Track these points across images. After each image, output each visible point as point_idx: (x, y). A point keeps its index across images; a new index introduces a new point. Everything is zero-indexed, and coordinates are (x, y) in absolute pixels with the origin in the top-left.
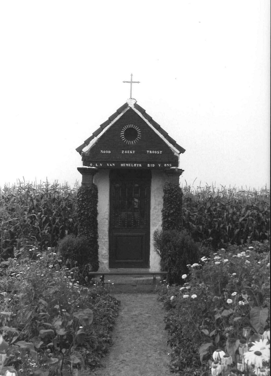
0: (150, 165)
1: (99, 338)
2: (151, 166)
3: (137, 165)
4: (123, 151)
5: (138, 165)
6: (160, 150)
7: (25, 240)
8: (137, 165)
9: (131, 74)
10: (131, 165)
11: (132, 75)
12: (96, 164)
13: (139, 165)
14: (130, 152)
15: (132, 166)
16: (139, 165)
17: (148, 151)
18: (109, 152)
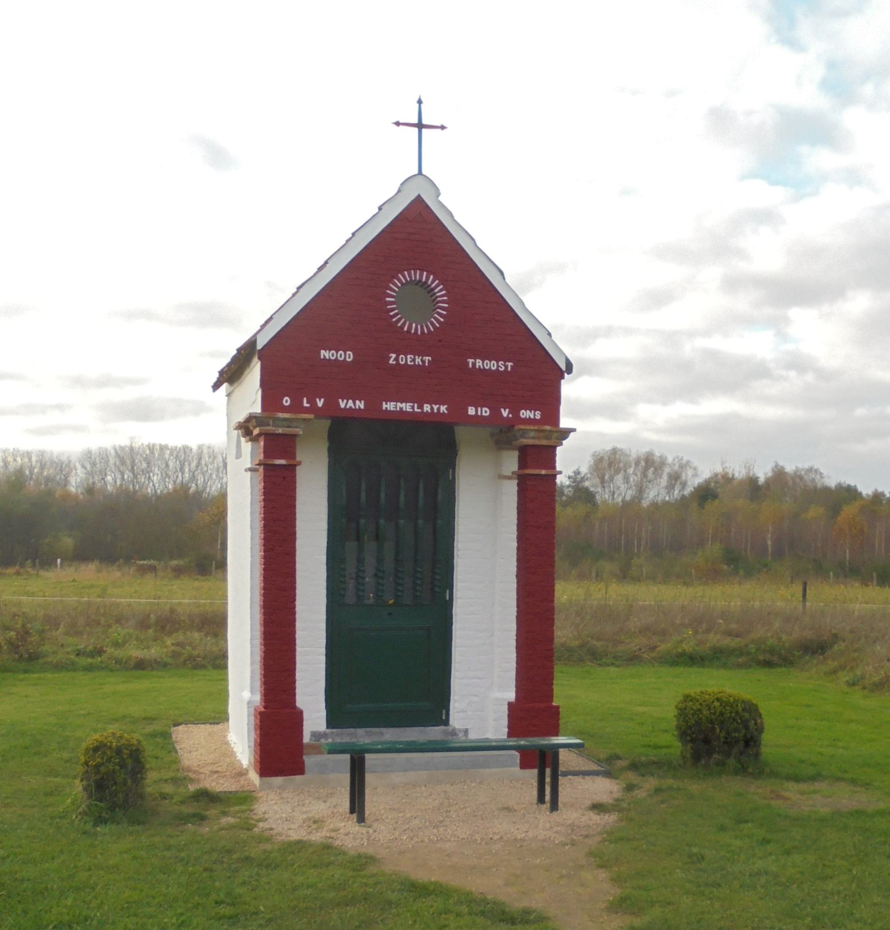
0: (476, 411)
1: (809, 98)
2: (479, 413)
3: (432, 409)
4: (394, 356)
5: (435, 407)
6: (422, 354)
7: (194, 648)
8: (432, 409)
9: (445, 125)
10: (413, 407)
11: (420, 102)
12: (305, 400)
13: (439, 409)
14: (414, 360)
15: (416, 410)
16: (439, 409)
17: (471, 361)
18: (325, 354)
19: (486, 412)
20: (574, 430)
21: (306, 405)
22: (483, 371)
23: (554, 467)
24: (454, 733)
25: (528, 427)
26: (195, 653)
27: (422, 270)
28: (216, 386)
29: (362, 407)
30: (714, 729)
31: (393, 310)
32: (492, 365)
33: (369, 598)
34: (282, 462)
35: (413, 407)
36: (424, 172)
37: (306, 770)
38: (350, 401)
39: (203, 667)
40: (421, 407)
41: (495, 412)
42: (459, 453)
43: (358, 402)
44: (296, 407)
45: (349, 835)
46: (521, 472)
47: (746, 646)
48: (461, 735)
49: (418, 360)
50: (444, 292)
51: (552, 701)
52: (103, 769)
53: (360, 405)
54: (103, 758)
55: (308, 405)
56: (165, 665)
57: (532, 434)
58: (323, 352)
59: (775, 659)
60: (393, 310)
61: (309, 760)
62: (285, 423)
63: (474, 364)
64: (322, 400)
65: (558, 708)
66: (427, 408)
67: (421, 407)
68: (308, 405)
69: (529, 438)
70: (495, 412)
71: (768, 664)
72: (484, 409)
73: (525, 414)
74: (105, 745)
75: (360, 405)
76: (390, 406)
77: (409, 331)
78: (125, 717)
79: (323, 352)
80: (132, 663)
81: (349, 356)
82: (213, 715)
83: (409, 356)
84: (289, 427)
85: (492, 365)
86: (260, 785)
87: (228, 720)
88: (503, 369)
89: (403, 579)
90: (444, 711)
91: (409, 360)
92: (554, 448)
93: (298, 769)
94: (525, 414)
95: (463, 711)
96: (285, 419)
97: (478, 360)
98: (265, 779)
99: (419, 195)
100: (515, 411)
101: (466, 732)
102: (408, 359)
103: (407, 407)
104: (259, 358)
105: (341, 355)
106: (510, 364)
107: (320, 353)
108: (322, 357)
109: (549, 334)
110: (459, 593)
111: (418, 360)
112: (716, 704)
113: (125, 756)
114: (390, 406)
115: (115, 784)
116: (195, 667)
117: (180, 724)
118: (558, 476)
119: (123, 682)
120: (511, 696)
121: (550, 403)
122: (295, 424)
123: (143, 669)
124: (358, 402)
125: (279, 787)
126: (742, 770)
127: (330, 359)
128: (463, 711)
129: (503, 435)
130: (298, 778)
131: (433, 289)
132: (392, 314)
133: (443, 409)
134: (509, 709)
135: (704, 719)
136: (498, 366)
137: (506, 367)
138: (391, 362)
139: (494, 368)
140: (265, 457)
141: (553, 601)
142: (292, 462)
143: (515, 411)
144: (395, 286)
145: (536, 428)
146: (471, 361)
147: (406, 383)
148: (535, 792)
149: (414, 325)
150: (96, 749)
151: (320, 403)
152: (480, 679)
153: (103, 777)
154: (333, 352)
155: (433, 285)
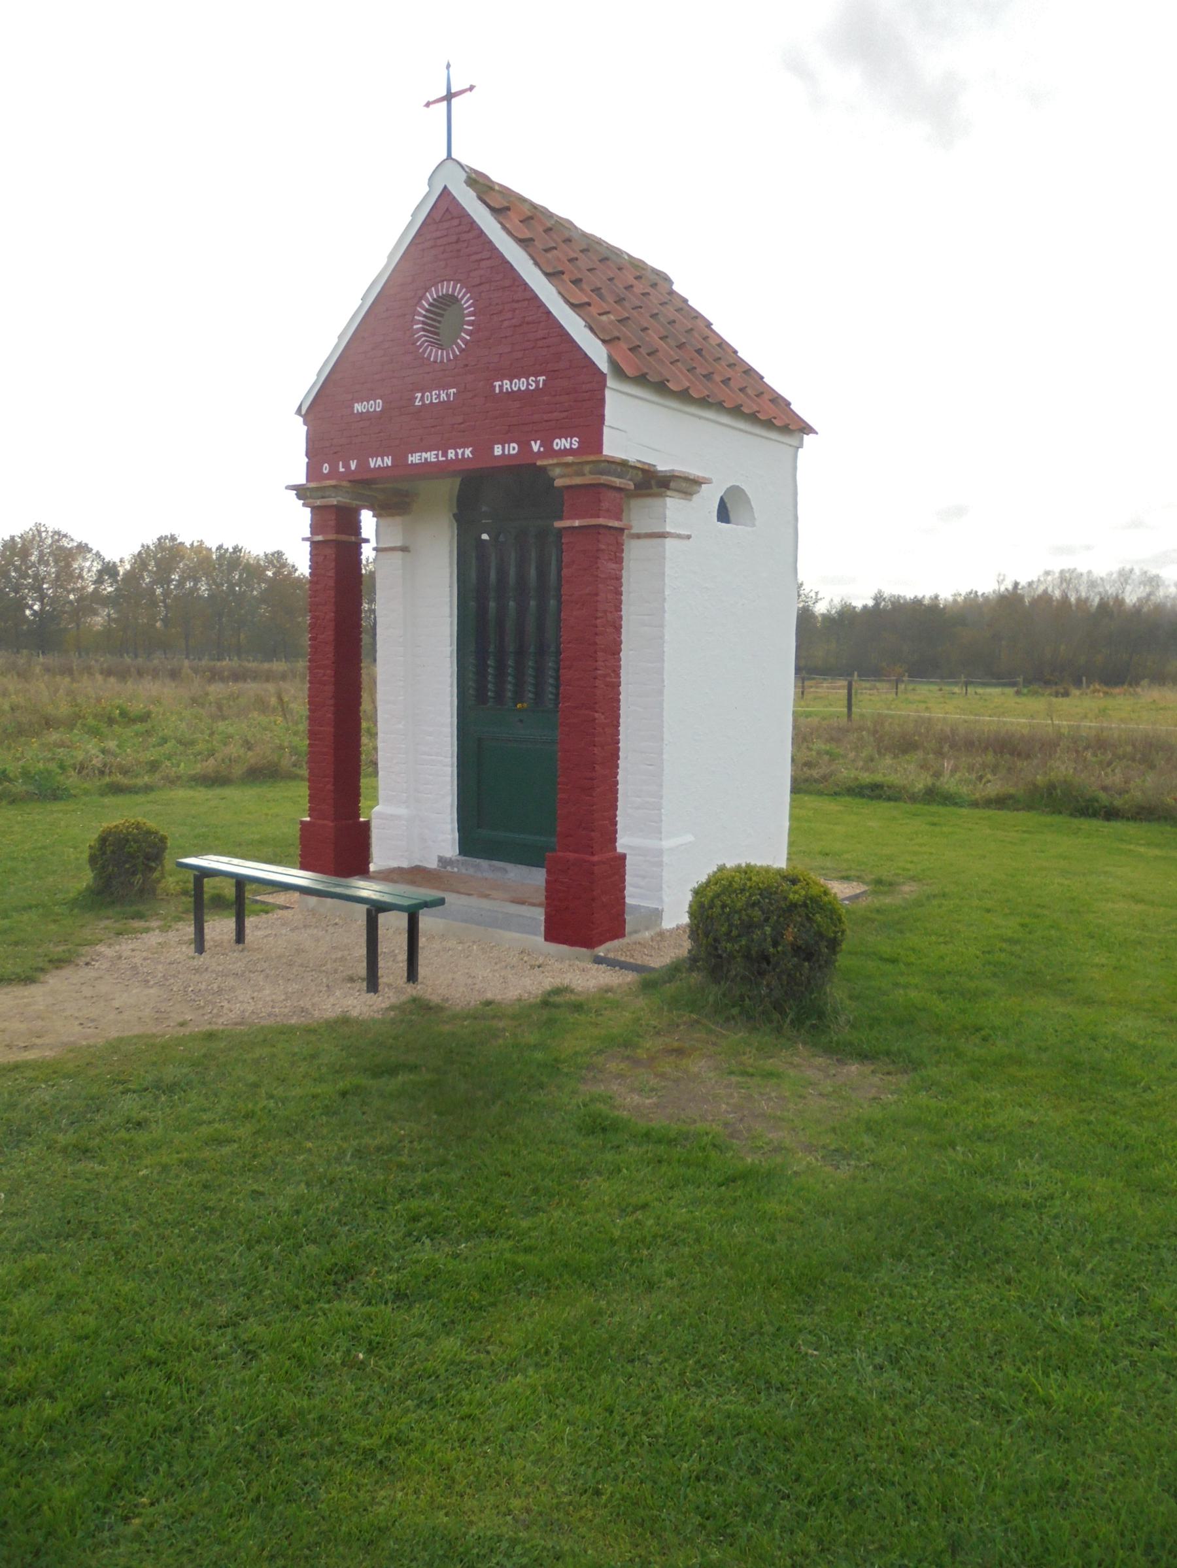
0: (503, 450)
3: (457, 454)
4: (419, 395)
5: (460, 452)
8: (457, 454)
10: (437, 456)
13: (463, 454)
14: (438, 396)
15: (441, 459)
16: (463, 454)
17: (497, 384)
18: (358, 407)
22: (510, 394)
28: (288, 488)
35: (437, 456)
36: (454, 156)
40: (445, 454)
41: (525, 446)
53: (388, 461)
63: (501, 387)
67: (445, 454)
72: (513, 445)
73: (560, 444)
75: (388, 461)
76: (414, 458)
100: (547, 444)
103: (431, 456)
111: (443, 396)
122: (327, 494)
136: (528, 384)
137: (537, 382)
143: (547, 444)
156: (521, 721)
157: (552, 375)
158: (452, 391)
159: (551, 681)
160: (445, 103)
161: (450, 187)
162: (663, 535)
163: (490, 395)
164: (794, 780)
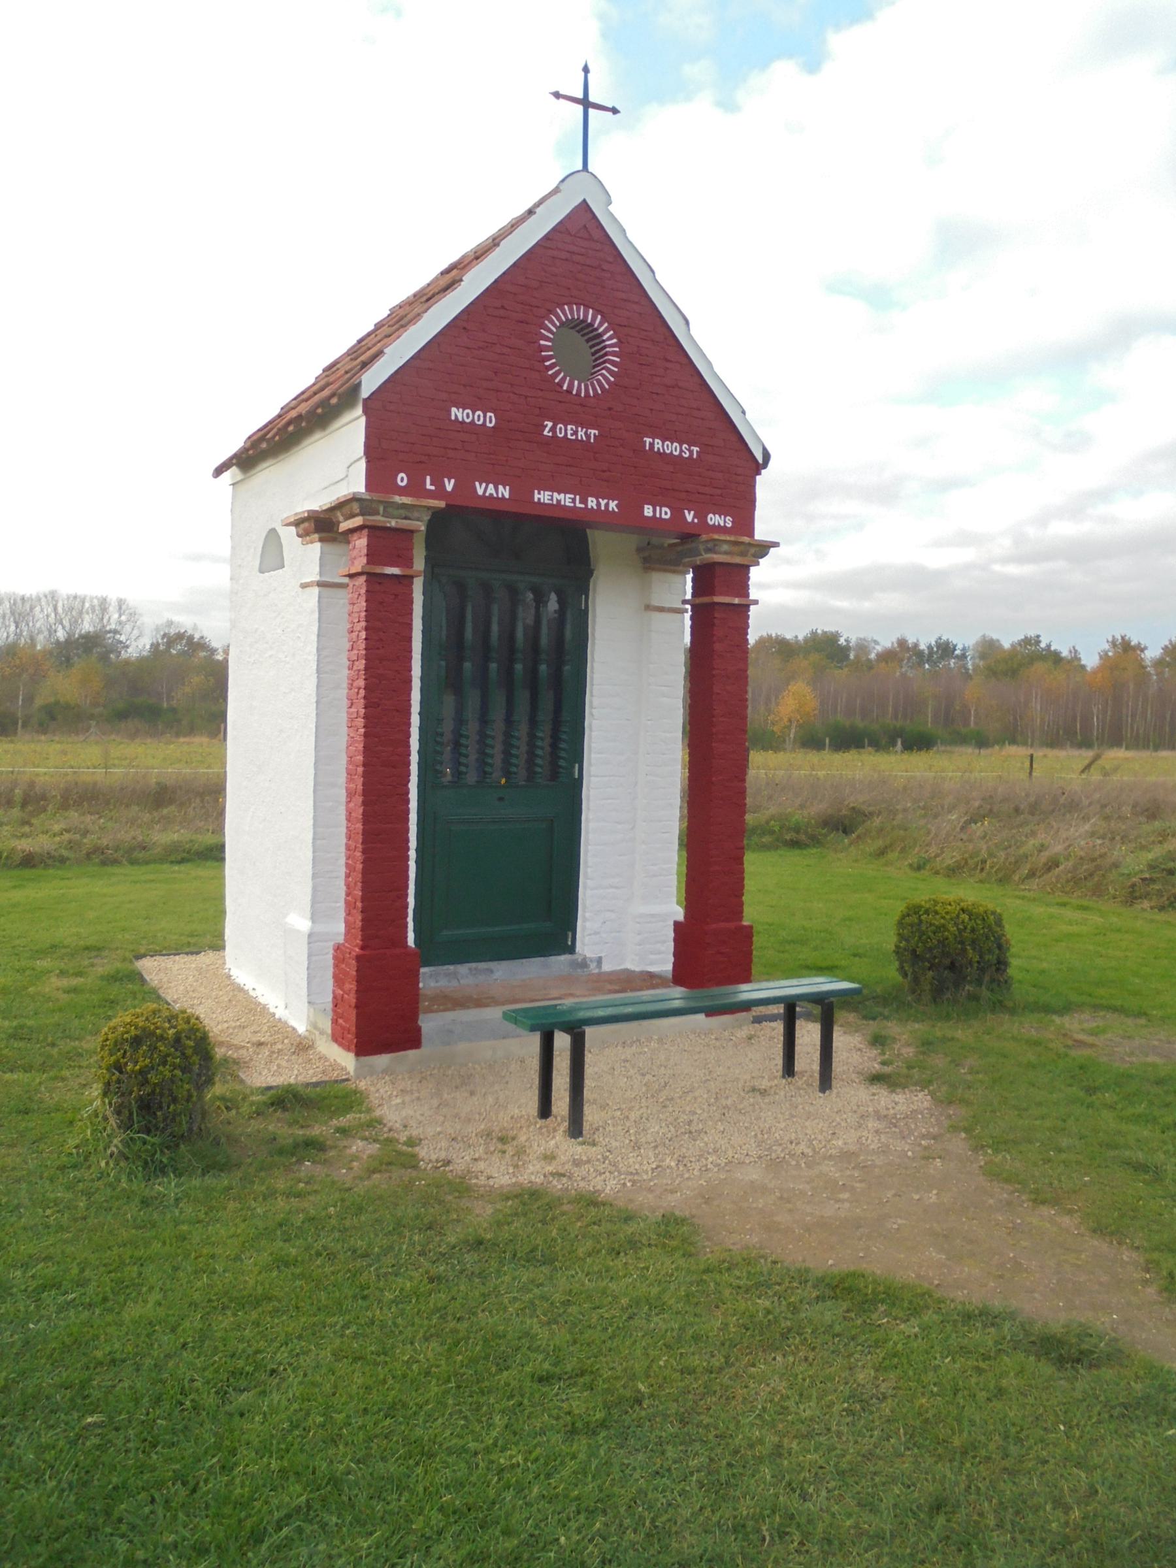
0: (654, 511)
3: (599, 504)
4: (550, 424)
5: (603, 502)
8: (599, 504)
9: (618, 107)
10: (574, 501)
12: (428, 478)
13: (607, 505)
14: (575, 433)
15: (578, 505)
16: (607, 505)
17: (648, 440)
18: (457, 413)
19: (665, 513)
20: (776, 545)
21: (429, 487)
22: (661, 455)
23: (748, 595)
24: (584, 964)
25: (723, 537)
26: (105, 842)
27: (587, 307)
28: (219, 471)
29: (507, 495)
30: (964, 950)
31: (549, 358)
32: (673, 448)
33: (445, 775)
34: (395, 571)
35: (574, 501)
36: (590, 169)
37: (424, 1040)
38: (491, 486)
39: (115, 862)
40: (584, 501)
41: (677, 513)
42: (595, 573)
43: (501, 488)
44: (414, 488)
45: (547, 1158)
46: (698, 601)
47: (767, 823)
48: (593, 966)
49: (581, 433)
50: (615, 341)
51: (741, 918)
52: (153, 1078)
53: (504, 492)
54: (151, 1058)
55: (433, 488)
56: (63, 860)
57: (725, 547)
58: (454, 410)
59: (803, 837)
60: (549, 358)
61: (428, 1024)
62: (403, 512)
63: (652, 445)
64: (453, 481)
65: (751, 927)
66: (592, 503)
67: (584, 501)
68: (433, 488)
69: (720, 553)
70: (677, 513)
71: (795, 844)
72: (664, 509)
73: (714, 519)
74: (153, 1034)
75: (504, 492)
76: (543, 497)
77: (569, 391)
78: (53, 946)
79: (454, 410)
80: (17, 858)
81: (491, 420)
82: (184, 939)
83: (569, 427)
84: (406, 518)
85: (673, 448)
86: (356, 1070)
87: (223, 948)
88: (687, 455)
89: (518, 748)
90: (570, 934)
91: (569, 432)
92: (746, 568)
93: (412, 1040)
94: (714, 519)
95: (596, 933)
96: (404, 506)
97: (657, 441)
98: (363, 1059)
99: (584, 200)
100: (701, 516)
101: (599, 961)
102: (567, 431)
103: (566, 499)
104: (365, 411)
105: (478, 417)
106: (695, 449)
107: (450, 411)
108: (453, 418)
109: (744, 412)
110: (593, 769)
111: (581, 433)
112: (965, 917)
113: (189, 1052)
114: (543, 497)
115: (175, 1100)
116: (104, 863)
117: (144, 956)
118: (752, 607)
119: (15, 887)
120: (679, 914)
121: (742, 506)
122: (416, 514)
123: (34, 866)
124: (501, 488)
125: (385, 1071)
126: (998, 1006)
127: (463, 422)
128: (596, 933)
129: (659, 553)
130: (411, 1054)
131: (600, 335)
132: (547, 363)
133: (613, 505)
134: (675, 931)
135: (951, 938)
136: (681, 451)
137: (691, 452)
138: (545, 433)
139: (676, 453)
140: (368, 563)
141: (744, 780)
142: (408, 572)
143: (701, 516)
144: (552, 325)
145: (732, 538)
146: (648, 440)
147: (569, 465)
148: (779, 1061)
149: (576, 383)
150: (136, 1041)
151: (449, 486)
152: (616, 888)
153: (153, 1092)
154: (469, 411)
155: (601, 330)
156: (501, 799)
157: (705, 448)
158: (593, 432)
159: (539, 761)
160: (591, 111)
161: (589, 201)
162: (320, 584)
163: (639, 450)
164: (224, 852)
